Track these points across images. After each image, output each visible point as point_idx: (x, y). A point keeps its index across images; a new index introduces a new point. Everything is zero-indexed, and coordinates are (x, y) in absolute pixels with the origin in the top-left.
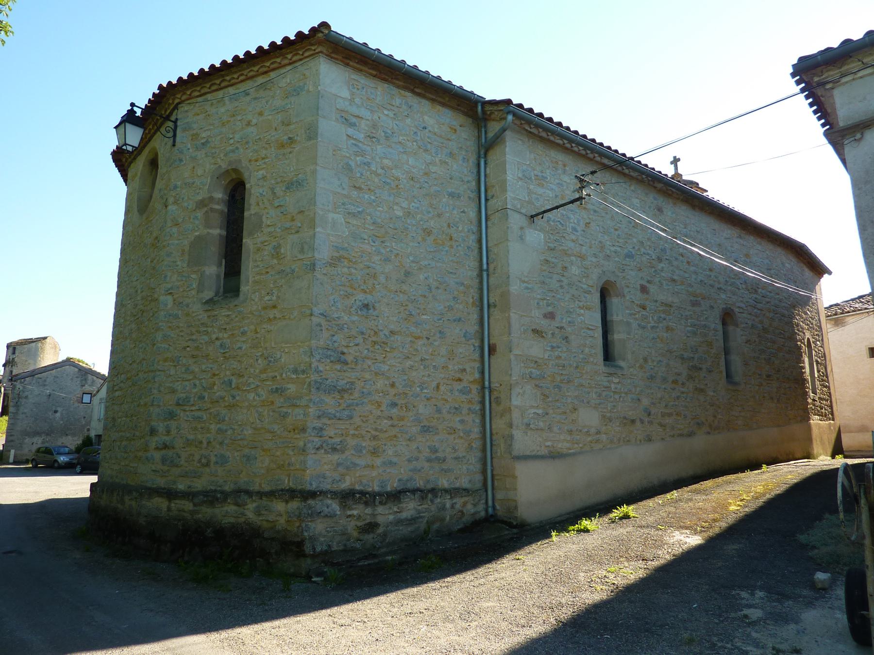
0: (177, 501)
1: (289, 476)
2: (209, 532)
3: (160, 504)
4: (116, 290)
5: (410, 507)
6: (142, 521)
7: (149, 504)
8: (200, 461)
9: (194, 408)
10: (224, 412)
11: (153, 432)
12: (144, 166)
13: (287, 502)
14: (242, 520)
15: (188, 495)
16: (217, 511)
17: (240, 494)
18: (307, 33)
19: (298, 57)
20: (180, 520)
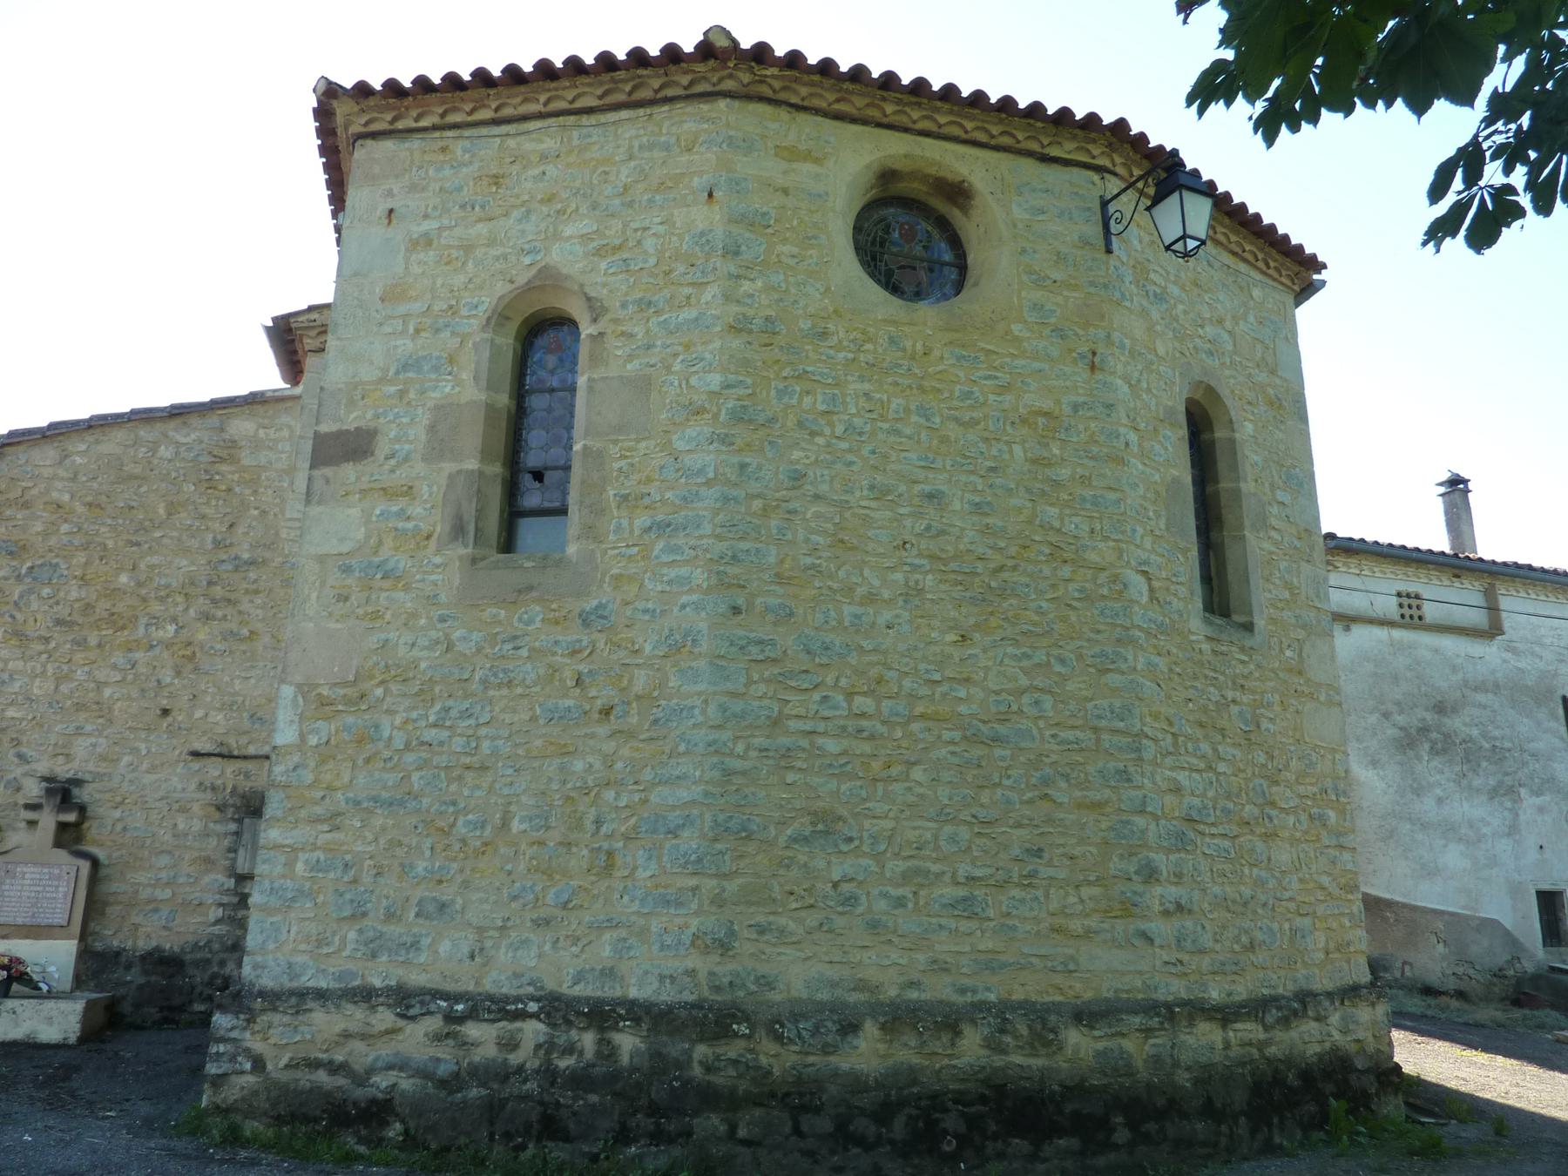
0: (1239, 1026)
1: (1348, 962)
2: (1292, 1078)
3: (1204, 1040)
4: (1499, 559)
5: (324, 1023)
6: (1183, 1079)
7: (1190, 1040)
8: (1237, 940)
9: (1214, 830)
10: (1260, 846)
11: (1150, 874)
12: (868, 167)
13: (1373, 1005)
14: (1328, 1045)
15: (1257, 1008)
16: (1294, 1034)
17: (1303, 1003)
18: (559, 65)
19: (1276, 275)
20: (1244, 1064)
